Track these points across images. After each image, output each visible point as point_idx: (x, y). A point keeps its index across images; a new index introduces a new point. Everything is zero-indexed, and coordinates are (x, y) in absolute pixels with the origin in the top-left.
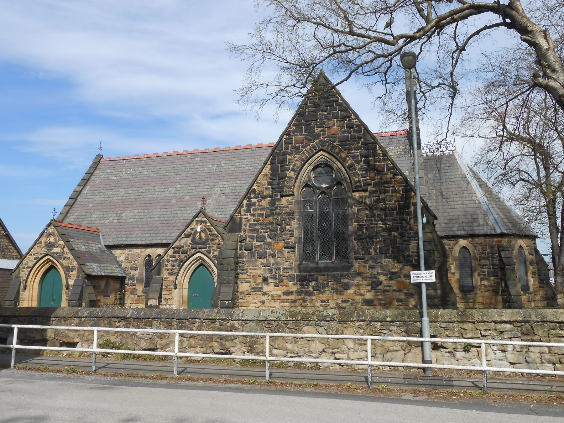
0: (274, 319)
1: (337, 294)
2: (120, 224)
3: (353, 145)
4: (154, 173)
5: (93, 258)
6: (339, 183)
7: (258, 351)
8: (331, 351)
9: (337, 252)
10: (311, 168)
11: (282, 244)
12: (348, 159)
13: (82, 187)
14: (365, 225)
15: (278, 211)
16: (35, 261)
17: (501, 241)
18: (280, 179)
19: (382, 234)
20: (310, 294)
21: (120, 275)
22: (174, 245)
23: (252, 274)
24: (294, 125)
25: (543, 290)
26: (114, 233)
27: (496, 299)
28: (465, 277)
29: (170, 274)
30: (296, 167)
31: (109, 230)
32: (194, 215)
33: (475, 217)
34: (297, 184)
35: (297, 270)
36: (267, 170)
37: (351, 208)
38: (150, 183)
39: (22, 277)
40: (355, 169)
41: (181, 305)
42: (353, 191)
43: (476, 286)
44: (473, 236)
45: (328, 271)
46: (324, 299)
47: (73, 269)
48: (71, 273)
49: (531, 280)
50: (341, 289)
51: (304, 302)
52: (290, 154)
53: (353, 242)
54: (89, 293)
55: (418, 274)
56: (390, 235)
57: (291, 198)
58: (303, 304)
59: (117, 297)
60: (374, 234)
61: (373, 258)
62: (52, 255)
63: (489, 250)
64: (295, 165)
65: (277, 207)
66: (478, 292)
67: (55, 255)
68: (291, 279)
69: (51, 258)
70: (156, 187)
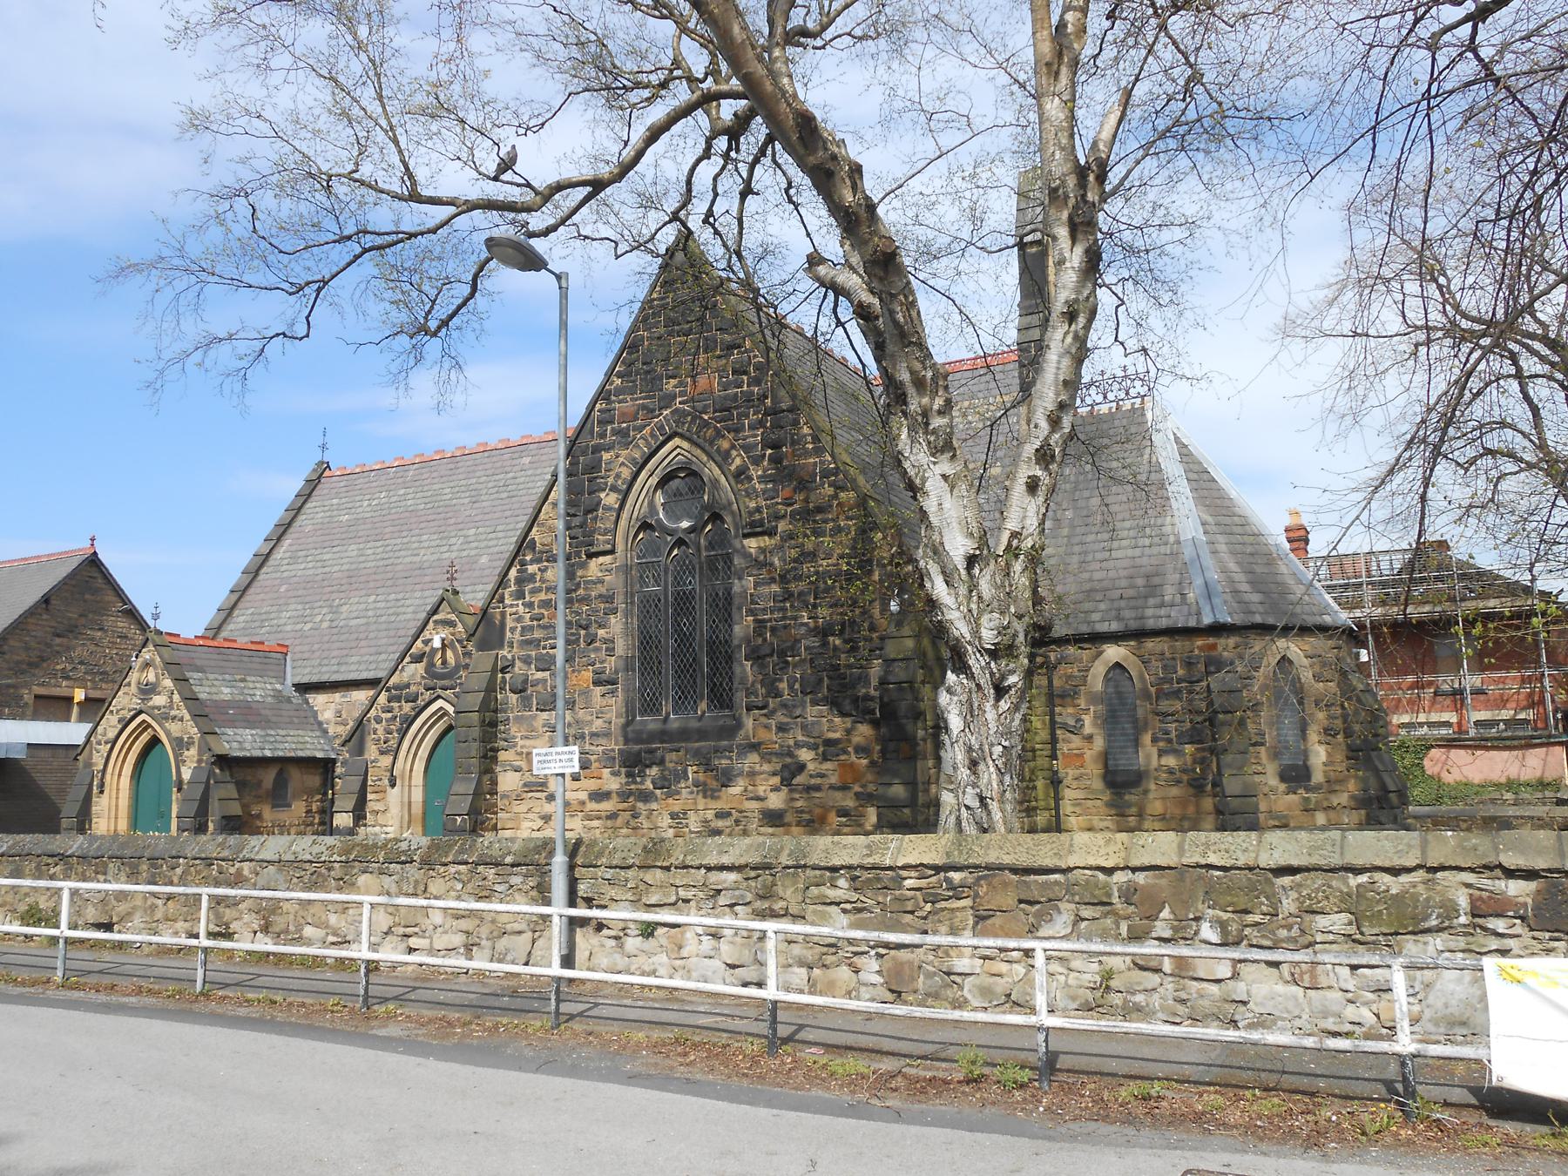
0: (309, 857)
1: (705, 797)
2: (335, 631)
3: (747, 416)
4: (427, 500)
5: (248, 714)
6: (716, 517)
7: (277, 930)
8: (401, 930)
9: (712, 690)
10: (654, 480)
11: (588, 675)
12: (734, 453)
13: (273, 543)
14: (770, 620)
15: (581, 592)
16: (120, 726)
17: (1213, 647)
18: (588, 512)
19: (808, 643)
20: (646, 797)
21: (320, 755)
22: (391, 683)
23: (525, 750)
24: (619, 375)
25: (1356, 777)
26: (317, 654)
27: (1197, 805)
28: (1121, 747)
29: (382, 753)
30: (620, 482)
31: (306, 648)
32: (429, 608)
33: (1156, 580)
34: (623, 523)
35: (621, 739)
36: (559, 493)
37: (740, 579)
38: (414, 526)
39: (96, 764)
40: (750, 479)
41: (405, 825)
42: (746, 536)
43: (1147, 772)
44: (1140, 635)
45: (687, 740)
46: (676, 809)
47: (190, 743)
48: (186, 753)
49: (1318, 753)
50: (714, 784)
51: (635, 817)
52: (608, 450)
53: (742, 665)
54: (225, 800)
55: (546, 754)
56: (825, 644)
57: (607, 559)
58: (632, 823)
59: (314, 808)
60: (789, 644)
61: (784, 706)
62: (150, 711)
63: (1181, 672)
64: (618, 476)
65: (579, 583)
66: (1152, 787)
67: (156, 711)
68: (608, 760)
69: (149, 720)
70: (425, 537)
